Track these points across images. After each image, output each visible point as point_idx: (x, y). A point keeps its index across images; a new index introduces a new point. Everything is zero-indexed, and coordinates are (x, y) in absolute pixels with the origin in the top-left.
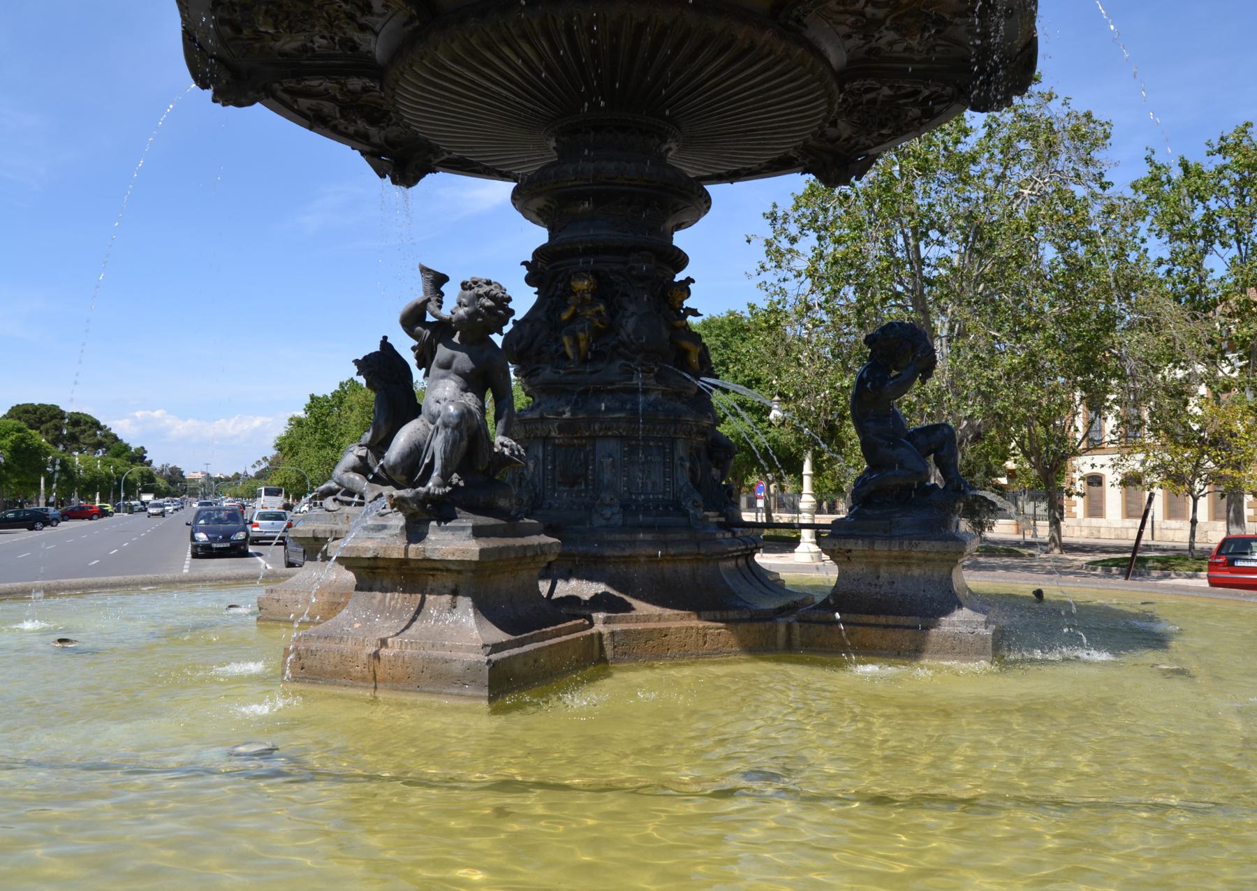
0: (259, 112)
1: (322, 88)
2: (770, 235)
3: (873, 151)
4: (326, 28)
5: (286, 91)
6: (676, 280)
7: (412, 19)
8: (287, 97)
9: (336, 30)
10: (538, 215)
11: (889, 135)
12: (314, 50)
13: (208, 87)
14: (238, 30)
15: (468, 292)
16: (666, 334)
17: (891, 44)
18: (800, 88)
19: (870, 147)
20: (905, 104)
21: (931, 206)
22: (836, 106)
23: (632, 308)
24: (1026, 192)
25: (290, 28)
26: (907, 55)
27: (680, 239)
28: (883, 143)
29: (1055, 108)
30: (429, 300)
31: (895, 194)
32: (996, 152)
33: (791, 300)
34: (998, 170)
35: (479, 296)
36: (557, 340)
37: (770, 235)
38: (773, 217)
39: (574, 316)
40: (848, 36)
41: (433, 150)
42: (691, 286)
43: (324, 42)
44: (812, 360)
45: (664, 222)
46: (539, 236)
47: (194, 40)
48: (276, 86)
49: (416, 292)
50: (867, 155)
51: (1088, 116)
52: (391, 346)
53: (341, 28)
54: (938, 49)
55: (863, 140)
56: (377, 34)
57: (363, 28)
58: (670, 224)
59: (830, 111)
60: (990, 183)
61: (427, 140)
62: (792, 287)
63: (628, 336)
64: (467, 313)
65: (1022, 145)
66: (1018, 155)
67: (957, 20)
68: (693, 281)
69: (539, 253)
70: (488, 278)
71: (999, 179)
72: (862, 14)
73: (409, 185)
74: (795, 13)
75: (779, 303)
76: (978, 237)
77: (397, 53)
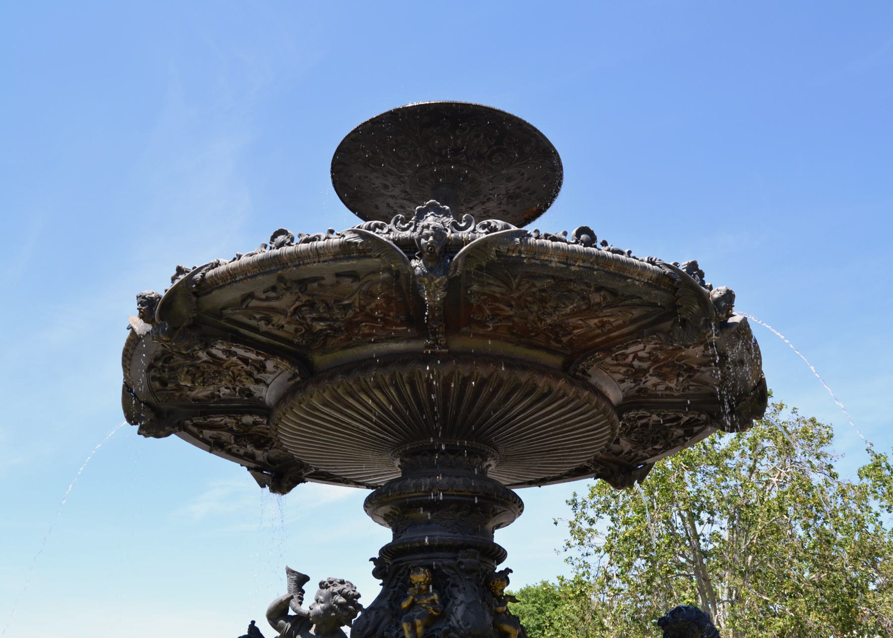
0: (174, 441)
1: (223, 422)
2: (573, 518)
3: (649, 461)
4: (230, 381)
5: (195, 425)
6: (497, 571)
7: (294, 376)
8: (195, 430)
9: (237, 383)
10: (385, 519)
11: (661, 450)
12: (219, 397)
13: (136, 424)
14: (164, 383)
15: (325, 591)
16: (489, 620)
17: (655, 385)
18: (588, 419)
19: (647, 458)
20: (671, 427)
21: (699, 491)
22: (618, 431)
23: (461, 597)
24: (775, 480)
25: (204, 383)
26: (668, 392)
27: (500, 537)
28: (657, 455)
29: (784, 416)
30: (292, 597)
31: (669, 484)
32: (747, 449)
33: (593, 572)
34: (750, 463)
35: (334, 594)
36: (398, 625)
37: (573, 518)
38: (574, 504)
39: (413, 604)
40: (622, 381)
41: (304, 466)
42: (510, 576)
43: (228, 391)
44: (614, 625)
45: (486, 524)
46: (385, 535)
47: (131, 391)
48: (188, 422)
49: (281, 590)
50: (645, 464)
51: (813, 421)
52: (257, 630)
53: (241, 382)
54: (691, 388)
55: (640, 452)
56: (268, 385)
57: (258, 381)
58: (490, 526)
59: (613, 435)
60: (744, 473)
61: (300, 460)
62: (593, 560)
63: (458, 622)
64: (323, 609)
65: (766, 443)
66: (763, 450)
67: (703, 369)
68: (511, 571)
69: (385, 551)
70: (342, 578)
71: (751, 470)
72: (632, 366)
73: (283, 493)
74: (581, 367)
75: (584, 575)
76: (741, 516)
77: (282, 399)
